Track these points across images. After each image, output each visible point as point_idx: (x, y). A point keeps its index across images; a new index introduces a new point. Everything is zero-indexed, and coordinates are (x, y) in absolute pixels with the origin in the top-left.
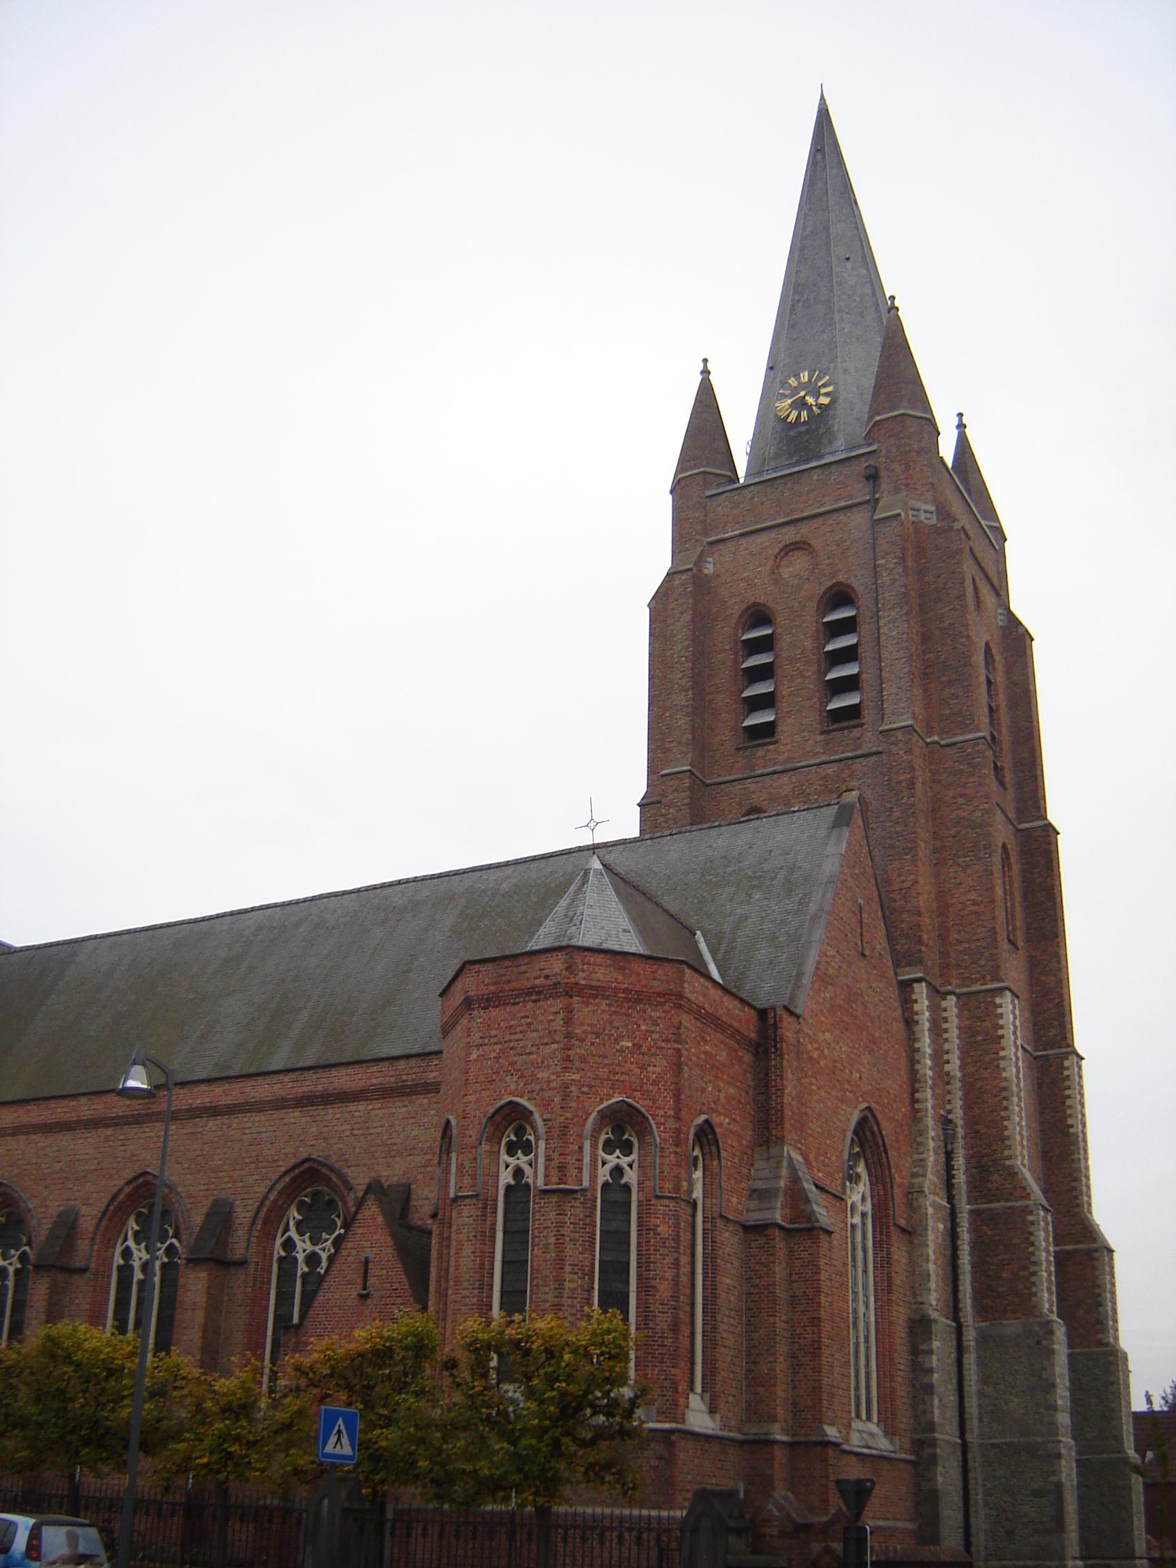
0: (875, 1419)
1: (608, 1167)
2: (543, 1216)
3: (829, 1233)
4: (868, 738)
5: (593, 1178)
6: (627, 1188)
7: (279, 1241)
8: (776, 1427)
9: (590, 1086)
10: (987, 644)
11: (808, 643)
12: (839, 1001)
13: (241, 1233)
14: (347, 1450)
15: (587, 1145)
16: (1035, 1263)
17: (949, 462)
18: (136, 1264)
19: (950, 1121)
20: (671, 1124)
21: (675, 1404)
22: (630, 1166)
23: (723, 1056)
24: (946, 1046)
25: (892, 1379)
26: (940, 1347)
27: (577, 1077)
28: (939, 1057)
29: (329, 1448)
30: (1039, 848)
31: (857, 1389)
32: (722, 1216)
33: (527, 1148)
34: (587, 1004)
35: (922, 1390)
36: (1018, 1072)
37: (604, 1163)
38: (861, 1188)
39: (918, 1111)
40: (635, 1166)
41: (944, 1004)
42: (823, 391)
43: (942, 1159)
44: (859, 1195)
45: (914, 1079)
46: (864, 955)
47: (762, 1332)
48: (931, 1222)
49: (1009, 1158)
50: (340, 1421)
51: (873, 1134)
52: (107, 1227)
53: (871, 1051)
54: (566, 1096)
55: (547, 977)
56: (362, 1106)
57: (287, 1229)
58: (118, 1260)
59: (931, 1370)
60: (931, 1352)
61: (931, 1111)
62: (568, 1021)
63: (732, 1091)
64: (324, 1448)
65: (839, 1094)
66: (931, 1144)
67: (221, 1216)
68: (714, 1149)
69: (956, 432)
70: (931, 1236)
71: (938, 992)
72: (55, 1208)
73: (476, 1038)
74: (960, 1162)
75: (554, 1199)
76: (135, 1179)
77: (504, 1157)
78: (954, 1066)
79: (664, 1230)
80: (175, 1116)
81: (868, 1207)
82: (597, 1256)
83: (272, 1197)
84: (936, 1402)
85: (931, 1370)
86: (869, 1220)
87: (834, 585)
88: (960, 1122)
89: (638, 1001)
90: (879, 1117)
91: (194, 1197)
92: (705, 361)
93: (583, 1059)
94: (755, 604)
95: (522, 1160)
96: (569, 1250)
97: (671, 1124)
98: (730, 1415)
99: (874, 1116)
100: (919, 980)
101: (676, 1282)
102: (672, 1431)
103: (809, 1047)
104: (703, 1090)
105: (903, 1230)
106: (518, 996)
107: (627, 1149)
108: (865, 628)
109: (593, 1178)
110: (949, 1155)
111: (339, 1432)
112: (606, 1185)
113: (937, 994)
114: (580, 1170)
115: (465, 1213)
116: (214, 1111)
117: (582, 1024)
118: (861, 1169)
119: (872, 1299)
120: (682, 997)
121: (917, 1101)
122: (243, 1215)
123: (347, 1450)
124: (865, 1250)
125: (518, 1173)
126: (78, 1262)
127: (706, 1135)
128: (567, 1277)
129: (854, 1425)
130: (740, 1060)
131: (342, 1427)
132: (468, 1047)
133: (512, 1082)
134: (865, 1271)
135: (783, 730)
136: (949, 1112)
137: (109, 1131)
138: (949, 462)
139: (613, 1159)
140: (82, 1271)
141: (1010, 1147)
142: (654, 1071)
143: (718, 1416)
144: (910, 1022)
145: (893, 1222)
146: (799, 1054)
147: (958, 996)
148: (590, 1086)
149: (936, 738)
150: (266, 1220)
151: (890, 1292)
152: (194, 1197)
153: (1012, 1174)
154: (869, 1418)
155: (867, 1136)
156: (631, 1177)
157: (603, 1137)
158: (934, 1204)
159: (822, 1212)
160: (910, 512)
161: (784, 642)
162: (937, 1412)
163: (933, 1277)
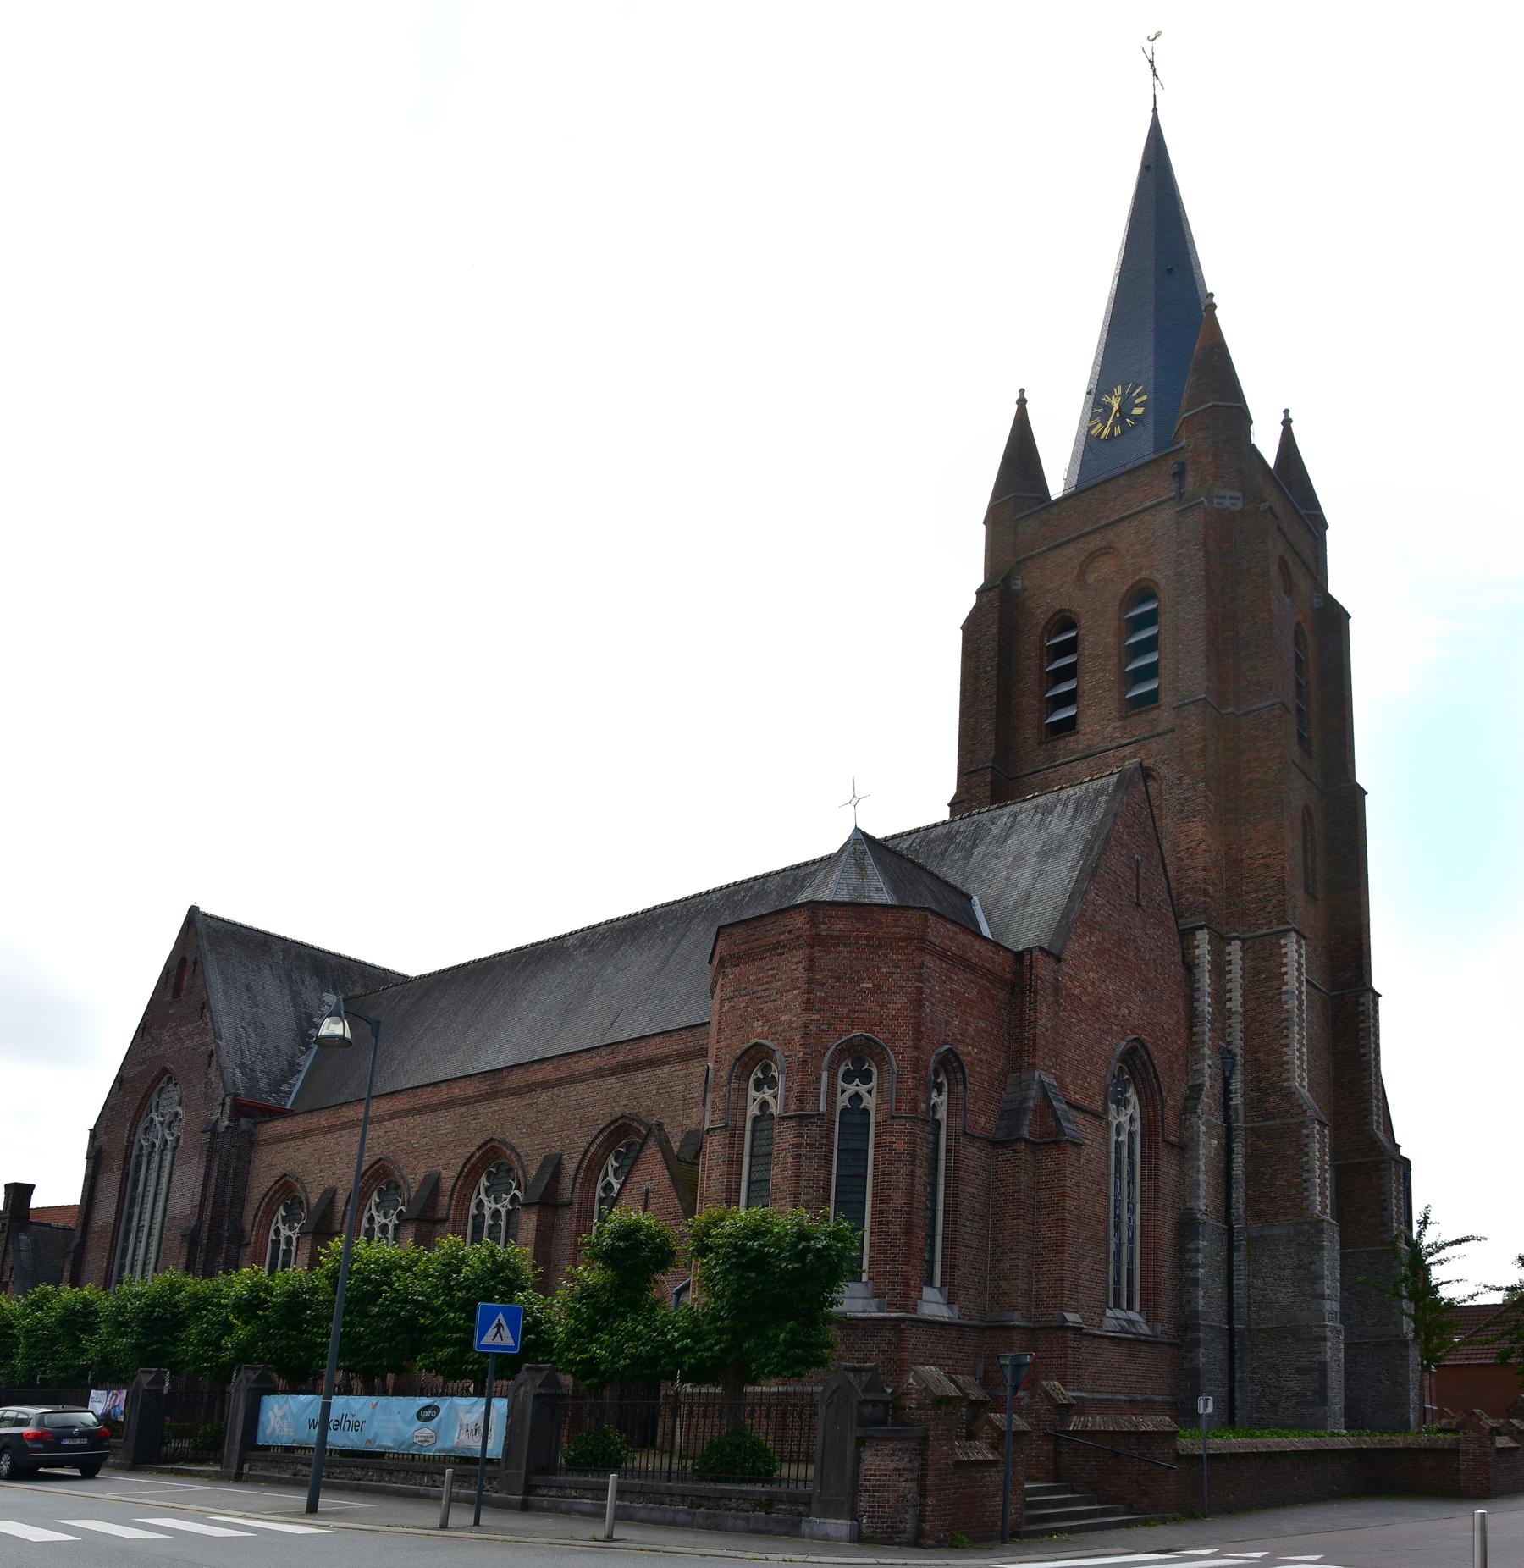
0: (1137, 1308)
1: (847, 1095)
2: (786, 1138)
3: (1078, 1145)
4: (1164, 716)
5: (831, 1103)
6: (866, 1112)
7: (600, 1185)
8: (1017, 1315)
9: (829, 1024)
10: (1299, 624)
11: (1110, 640)
12: (1107, 945)
13: (568, 1181)
14: (508, 1341)
15: (824, 1075)
16: (1308, 1171)
17: (1270, 458)
18: (487, 1213)
19: (1230, 1051)
20: (910, 1053)
21: (907, 1297)
22: (870, 1092)
23: (972, 994)
24: (1229, 986)
25: (1156, 1274)
26: (1206, 1248)
27: (816, 1017)
28: (1220, 996)
29: (487, 1340)
30: (1346, 808)
31: (1117, 1282)
32: (965, 1134)
33: (772, 1083)
34: (828, 952)
35: (1185, 1283)
36: (1301, 1004)
37: (843, 1091)
38: (1130, 1111)
39: (1195, 1043)
40: (874, 1092)
41: (1228, 949)
42: (1137, 401)
43: (1219, 1084)
44: (1127, 1117)
45: (1192, 1015)
46: (1138, 905)
47: (1006, 1233)
48: (1203, 1138)
49: (1287, 1080)
50: (500, 1316)
51: (1143, 1062)
52: (463, 1186)
53: (1143, 990)
54: (806, 1035)
55: (790, 932)
56: (666, 1069)
57: (606, 1175)
58: (473, 1211)
59: (1197, 1266)
60: (1197, 1250)
61: (1208, 1042)
62: (810, 969)
63: (982, 1024)
64: (481, 1338)
65: (1103, 1027)
66: (1207, 1071)
67: (554, 1165)
68: (959, 1076)
69: (1013, 409)
70: (1202, 1151)
71: (1223, 938)
72: (422, 1173)
73: (728, 993)
74: (1237, 1085)
75: (792, 1124)
76: (484, 1144)
77: (752, 1093)
78: (1236, 1003)
79: (900, 1146)
80: (513, 1092)
81: (1137, 1127)
82: (834, 1171)
83: (592, 1150)
84: (1201, 1293)
85: (1197, 1266)
86: (1138, 1138)
87: (1138, 582)
88: (1239, 1051)
89: (880, 947)
90: (1150, 1047)
91: (530, 1152)
92: (1022, 391)
93: (823, 1001)
94: (1060, 611)
95: (767, 1094)
96: (804, 1168)
97: (910, 1053)
98: (971, 1306)
99: (1143, 1046)
100: (1201, 928)
101: (910, 1191)
102: (902, 1320)
103: (1069, 984)
104: (948, 1023)
105: (1172, 1145)
106: (765, 951)
107: (866, 1078)
108: (1164, 619)
109: (831, 1103)
110: (1227, 1082)
111: (499, 1325)
112: (844, 1111)
113: (1220, 942)
114: (818, 1097)
115: (715, 1142)
116: (545, 1085)
117: (823, 970)
118: (1131, 1094)
119: (1138, 1206)
120: (924, 940)
121: (1195, 1034)
122: (570, 1166)
123: (508, 1341)
124: (1131, 1163)
125: (764, 1105)
126: (441, 1214)
127: (950, 1064)
128: (802, 1190)
129: (1109, 1313)
130: (992, 997)
131: (503, 1322)
132: (722, 1000)
133: (759, 1027)
134: (1131, 1182)
135: (1084, 725)
136: (1229, 1043)
137: (464, 1109)
138: (1270, 458)
139: (851, 1088)
140: (444, 1221)
141: (1288, 1071)
142: (893, 1008)
143: (956, 1307)
144: (1189, 966)
145: (1163, 1139)
146: (1056, 991)
147: (1243, 941)
148: (829, 1024)
149: (1231, 709)
150: (588, 1168)
151: (1156, 1198)
152: (530, 1152)
153: (1289, 1094)
154: (1130, 1307)
155: (1136, 1066)
156: (870, 1102)
157: (843, 1069)
158: (1207, 1123)
159: (1075, 1125)
160: (1215, 501)
161: (1086, 644)
162: (1201, 1302)
163: (1203, 1186)
